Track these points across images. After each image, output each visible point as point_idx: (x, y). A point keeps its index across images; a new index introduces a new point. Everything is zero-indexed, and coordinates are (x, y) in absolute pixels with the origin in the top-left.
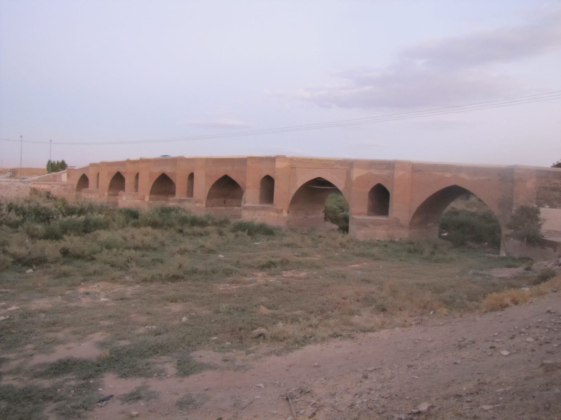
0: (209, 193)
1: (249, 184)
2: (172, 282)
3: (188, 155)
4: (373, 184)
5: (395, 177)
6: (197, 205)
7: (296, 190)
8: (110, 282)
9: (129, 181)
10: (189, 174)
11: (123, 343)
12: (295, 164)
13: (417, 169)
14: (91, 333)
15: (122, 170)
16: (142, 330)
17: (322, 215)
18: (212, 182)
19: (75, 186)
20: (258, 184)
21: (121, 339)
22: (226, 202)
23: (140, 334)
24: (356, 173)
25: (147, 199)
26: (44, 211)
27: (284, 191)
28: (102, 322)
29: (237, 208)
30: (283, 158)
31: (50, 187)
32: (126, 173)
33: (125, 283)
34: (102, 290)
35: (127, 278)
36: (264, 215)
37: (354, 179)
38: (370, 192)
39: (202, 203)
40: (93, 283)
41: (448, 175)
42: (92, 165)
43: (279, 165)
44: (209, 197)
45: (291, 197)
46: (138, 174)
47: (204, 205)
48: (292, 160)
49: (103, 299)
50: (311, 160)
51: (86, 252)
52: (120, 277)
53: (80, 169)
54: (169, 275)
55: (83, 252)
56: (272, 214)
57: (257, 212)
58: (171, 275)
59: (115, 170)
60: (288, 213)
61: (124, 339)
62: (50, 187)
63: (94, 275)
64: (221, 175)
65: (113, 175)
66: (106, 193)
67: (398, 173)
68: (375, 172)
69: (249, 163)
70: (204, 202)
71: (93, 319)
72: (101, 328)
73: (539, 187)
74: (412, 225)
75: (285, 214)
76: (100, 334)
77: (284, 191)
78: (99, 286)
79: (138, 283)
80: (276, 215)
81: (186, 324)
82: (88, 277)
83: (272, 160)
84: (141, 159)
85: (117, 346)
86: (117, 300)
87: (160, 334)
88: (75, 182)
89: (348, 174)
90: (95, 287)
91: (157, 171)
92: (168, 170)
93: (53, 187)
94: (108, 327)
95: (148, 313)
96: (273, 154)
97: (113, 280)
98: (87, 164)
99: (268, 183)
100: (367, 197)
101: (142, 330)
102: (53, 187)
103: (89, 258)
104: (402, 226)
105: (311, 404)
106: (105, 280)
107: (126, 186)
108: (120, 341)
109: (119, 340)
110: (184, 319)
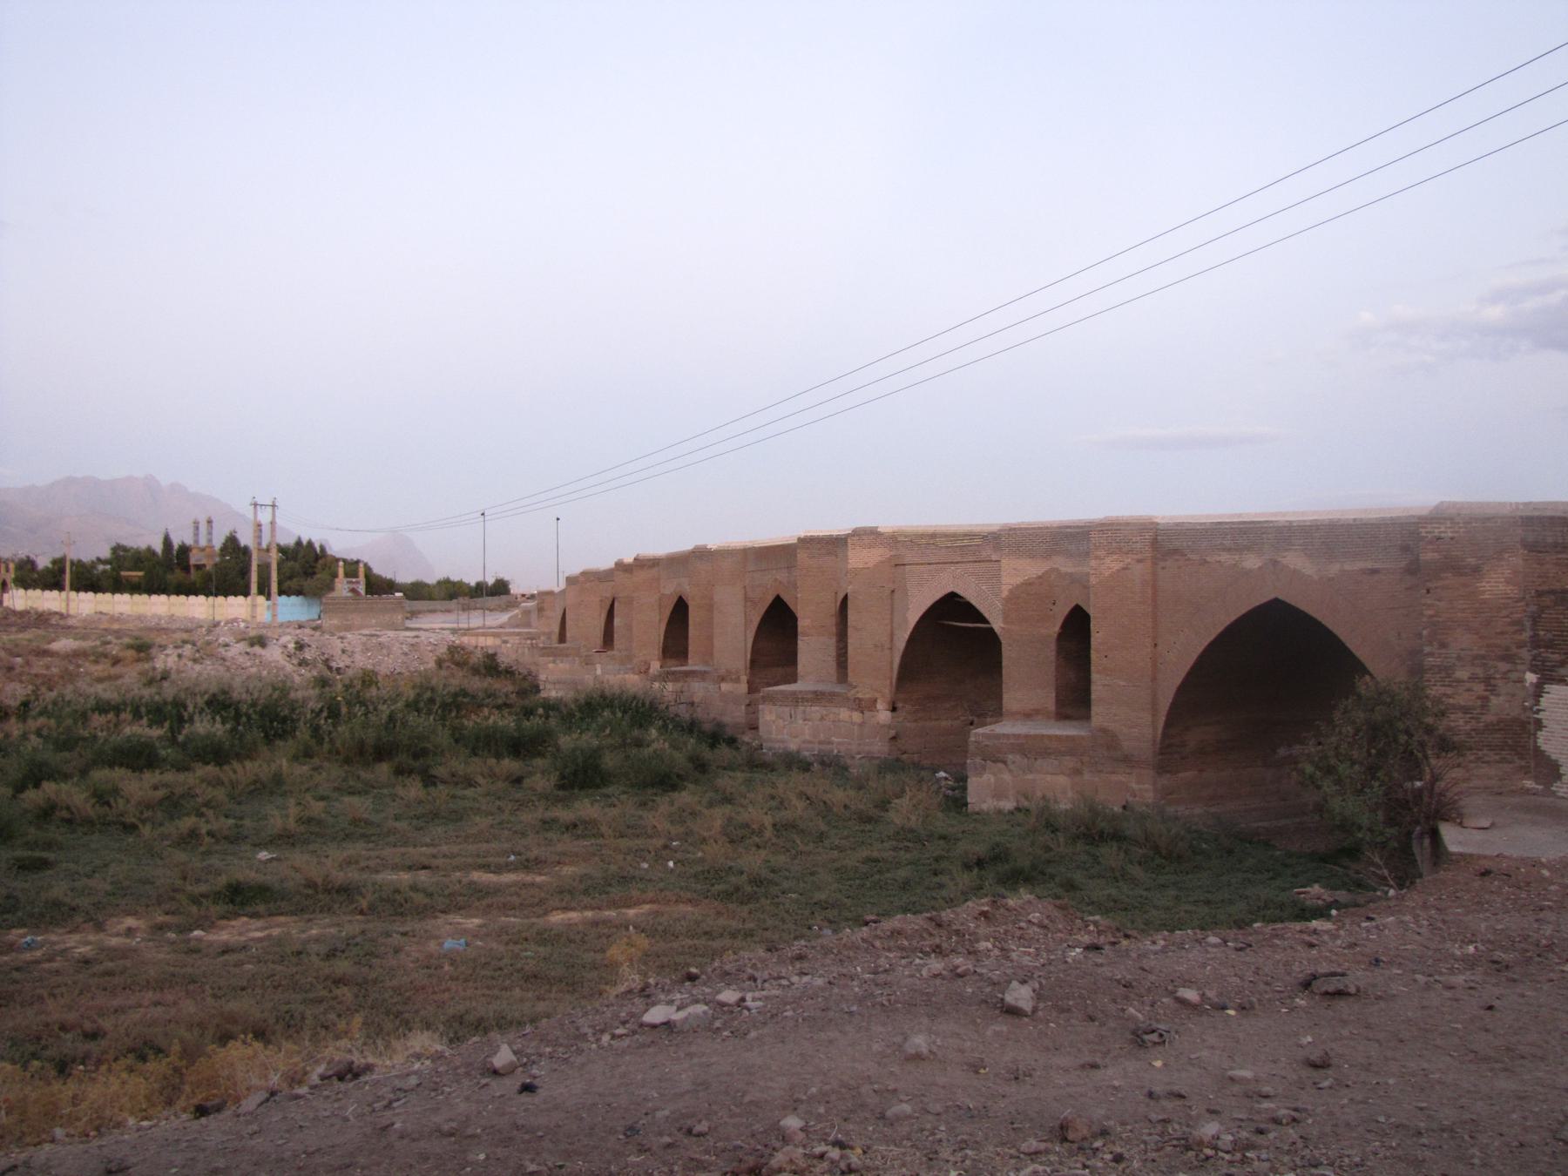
0: (754, 651)
6: (725, 687)
8: (160, 630)
13: (1164, 545)
25: (655, 666)
26: (286, 712)
30: (868, 536)
31: (498, 642)
36: (822, 719)
39: (737, 680)
41: (1252, 562)
47: (743, 687)
48: (894, 540)
50: (933, 536)
56: (844, 714)
57: (801, 708)
60: (894, 709)
62: (498, 642)
69: (802, 556)
70: (744, 678)
73: (1539, 594)
74: (1168, 754)
75: (883, 715)
80: (857, 717)
84: (584, 574)
93: (505, 642)
99: (778, 623)
102: (505, 642)
104: (1127, 760)
105: (313, 742)
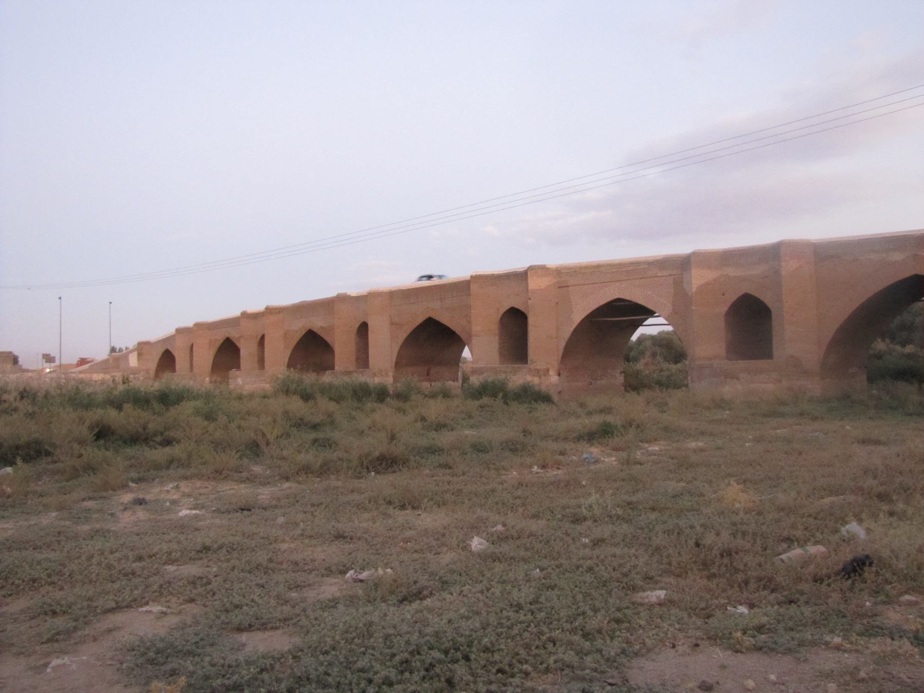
1: (476, 328)
2: (378, 472)
3: (354, 289)
4: (732, 297)
5: (783, 273)
7: (572, 329)
9: (247, 350)
10: (357, 326)
11: (259, 644)
12: (566, 279)
14: (118, 608)
15: (233, 334)
16: (331, 588)
17: (620, 379)
18: (403, 335)
19: (152, 373)
20: (495, 327)
21: (250, 628)
22: (431, 372)
23: (333, 603)
24: (698, 278)
27: (548, 335)
28: (171, 568)
29: (451, 382)
32: (239, 338)
33: (251, 480)
34: (184, 495)
35: (257, 469)
37: (694, 289)
38: (728, 314)
40: (162, 483)
42: (179, 331)
43: (534, 283)
44: (398, 365)
45: (563, 344)
46: (263, 337)
48: (559, 272)
49: (184, 512)
51: (150, 426)
52: (238, 470)
53: (159, 342)
54: (367, 455)
55: (144, 428)
58: (377, 454)
59: (220, 337)
60: (559, 375)
61: (264, 627)
63: (168, 468)
64: (420, 320)
65: (218, 344)
66: (207, 379)
67: (789, 266)
68: (732, 272)
69: (474, 287)
70: (391, 374)
71: (140, 558)
72: (164, 591)
76: (156, 608)
77: (548, 335)
78: (177, 487)
79: (287, 479)
81: (483, 557)
82: (149, 473)
83: (521, 276)
85: (231, 658)
86: (228, 512)
87: (419, 595)
88: (153, 365)
89: (678, 284)
90: (164, 491)
91: (298, 327)
92: (318, 323)
94: (193, 582)
95: (340, 536)
96: (519, 265)
97: (219, 474)
98: (171, 331)
99: (515, 322)
100: (721, 324)
101: (331, 588)
103: (159, 439)
106: (200, 476)
107: (242, 361)
108: (244, 637)
109: (240, 629)
110: (477, 543)
